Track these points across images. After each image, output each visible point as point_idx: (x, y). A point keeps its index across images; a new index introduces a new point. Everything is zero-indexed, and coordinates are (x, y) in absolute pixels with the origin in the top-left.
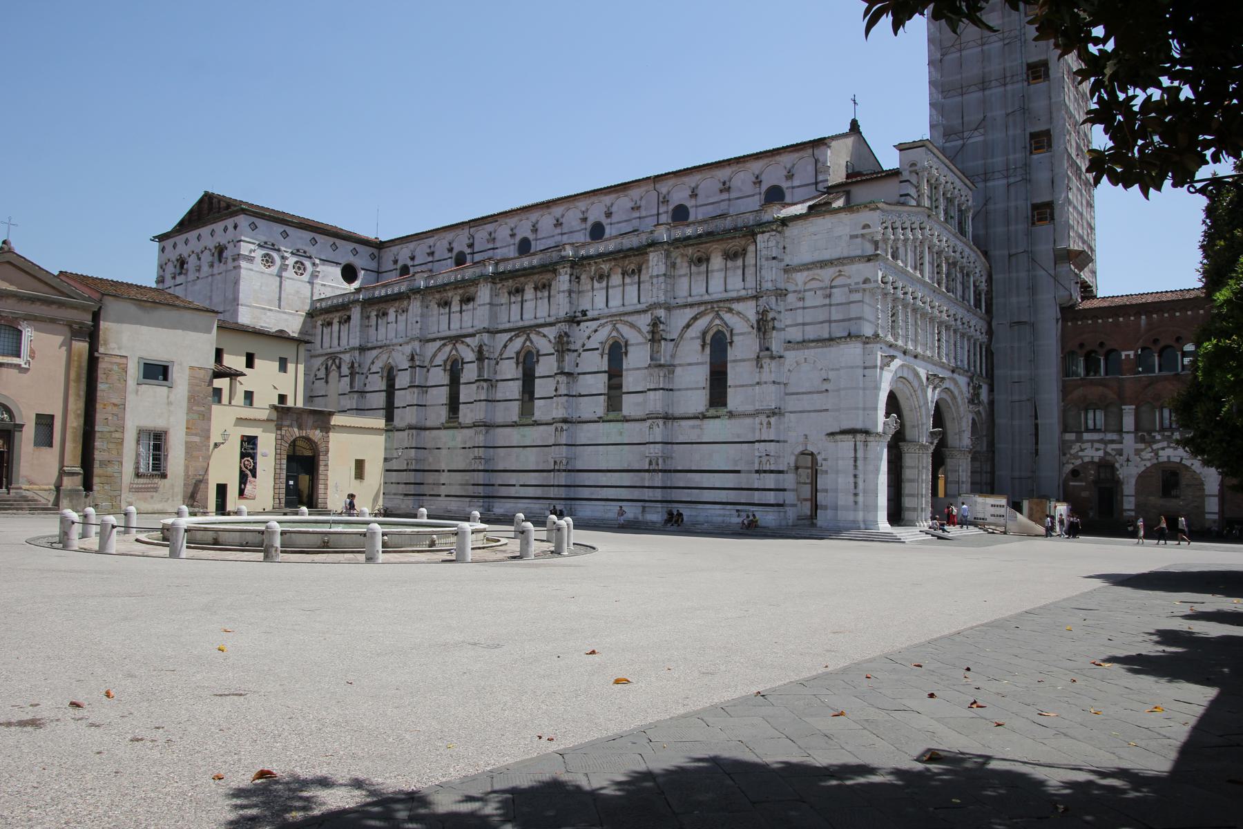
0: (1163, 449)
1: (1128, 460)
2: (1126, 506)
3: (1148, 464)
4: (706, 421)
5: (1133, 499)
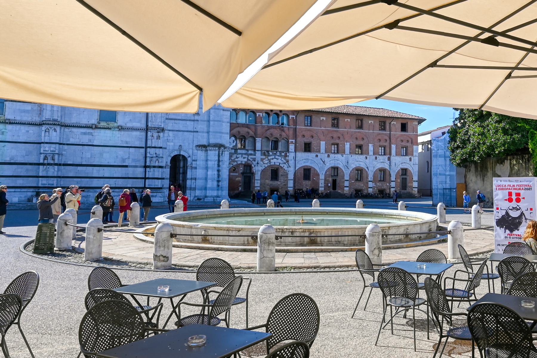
0: (273, 159)
1: (258, 163)
2: (256, 185)
3: (266, 166)
4: (97, 131)
5: (259, 181)
